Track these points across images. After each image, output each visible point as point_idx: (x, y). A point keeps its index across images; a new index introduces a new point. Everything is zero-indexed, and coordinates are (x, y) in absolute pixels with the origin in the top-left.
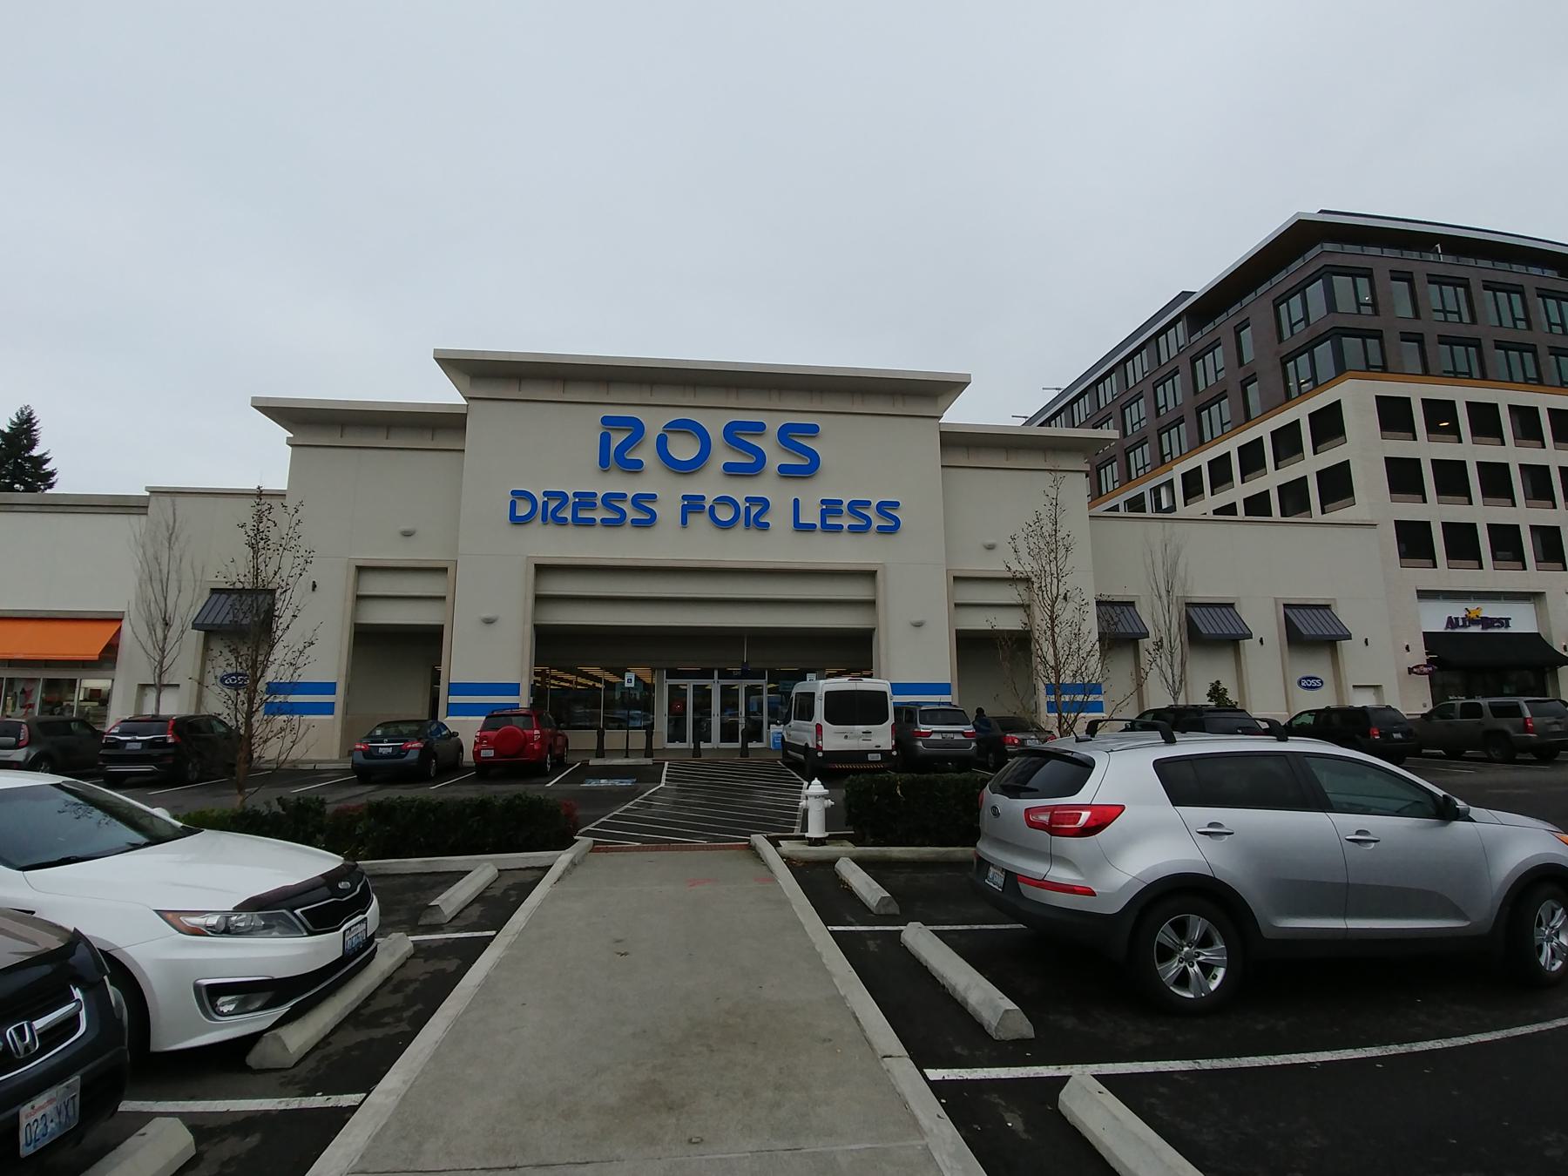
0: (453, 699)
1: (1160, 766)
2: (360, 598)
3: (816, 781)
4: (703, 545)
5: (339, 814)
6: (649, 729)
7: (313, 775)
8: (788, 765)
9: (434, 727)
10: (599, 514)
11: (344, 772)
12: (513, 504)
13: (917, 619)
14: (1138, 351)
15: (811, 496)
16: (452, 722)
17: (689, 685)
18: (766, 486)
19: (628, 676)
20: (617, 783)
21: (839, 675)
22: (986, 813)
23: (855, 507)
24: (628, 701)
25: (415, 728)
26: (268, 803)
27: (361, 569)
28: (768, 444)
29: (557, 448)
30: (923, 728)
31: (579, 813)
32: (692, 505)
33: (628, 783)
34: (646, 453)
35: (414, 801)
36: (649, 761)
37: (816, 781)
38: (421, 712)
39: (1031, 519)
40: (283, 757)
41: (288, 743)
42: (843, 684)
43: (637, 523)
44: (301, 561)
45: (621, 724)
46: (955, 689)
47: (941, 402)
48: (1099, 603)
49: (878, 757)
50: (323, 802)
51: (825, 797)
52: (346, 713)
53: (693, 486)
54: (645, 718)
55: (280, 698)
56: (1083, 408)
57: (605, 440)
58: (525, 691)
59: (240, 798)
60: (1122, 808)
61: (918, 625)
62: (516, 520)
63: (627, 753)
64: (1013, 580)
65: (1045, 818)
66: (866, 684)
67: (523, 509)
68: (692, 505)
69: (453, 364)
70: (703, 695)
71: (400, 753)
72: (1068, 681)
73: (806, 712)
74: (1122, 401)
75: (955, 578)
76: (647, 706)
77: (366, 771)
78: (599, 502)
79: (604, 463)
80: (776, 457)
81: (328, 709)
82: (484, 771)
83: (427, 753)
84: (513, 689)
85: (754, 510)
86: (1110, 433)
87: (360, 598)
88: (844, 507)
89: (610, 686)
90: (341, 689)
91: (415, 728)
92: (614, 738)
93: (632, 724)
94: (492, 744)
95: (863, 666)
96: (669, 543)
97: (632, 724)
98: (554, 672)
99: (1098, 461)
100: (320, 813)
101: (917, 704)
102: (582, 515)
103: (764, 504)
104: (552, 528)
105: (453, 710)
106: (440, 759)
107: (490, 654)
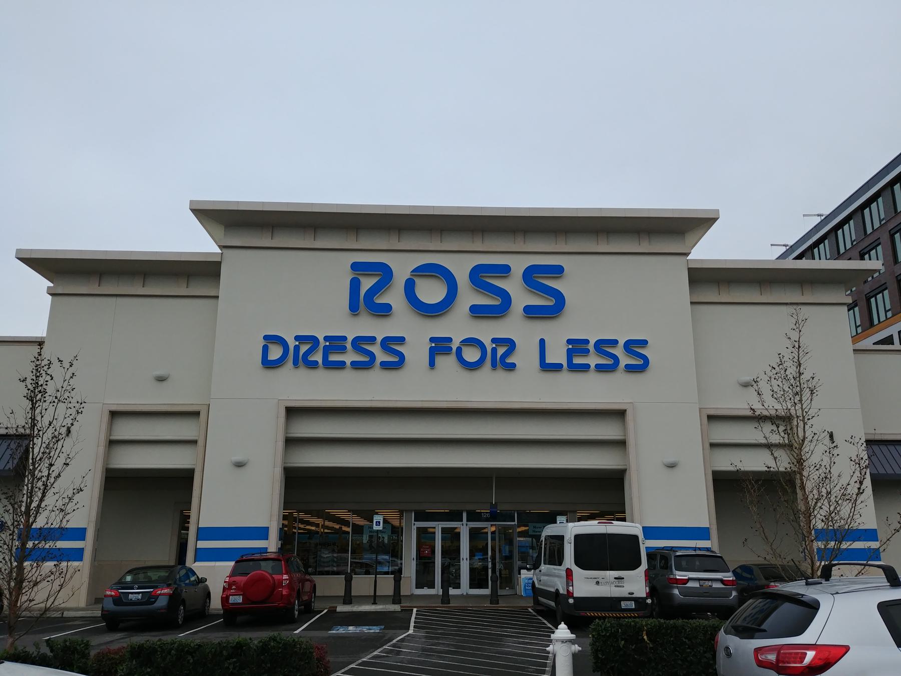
0: (202, 544)
1: (884, 608)
2: (112, 443)
3: (563, 626)
4: (450, 386)
5: (100, 657)
6: (398, 574)
7: (62, 622)
8: (539, 612)
9: (183, 572)
10: (349, 357)
11: (93, 620)
12: (265, 350)
13: (671, 460)
14: (846, 220)
15: (557, 336)
16: (201, 568)
17: (438, 527)
18: (512, 327)
19: (378, 518)
20: (365, 629)
21: (591, 517)
22: (721, 654)
23: (602, 346)
24: (377, 546)
25: (163, 574)
26: (37, 645)
27: (114, 415)
28: (513, 286)
29: (311, 294)
30: (680, 575)
31: (330, 658)
32: (440, 346)
33: (375, 630)
34: (394, 297)
35: (173, 643)
36: (397, 608)
37: (563, 626)
38: (167, 557)
39: (775, 362)
40: (847, 527)
41: (56, 587)
42: (592, 527)
43: (385, 366)
44: (73, 411)
45: (367, 569)
46: (714, 533)
47: (690, 238)
48: (869, 442)
49: (632, 605)
50: (87, 645)
51: (572, 642)
52: (95, 557)
53: (439, 328)
54: (393, 564)
55: (49, 545)
56: (849, 234)
57: (355, 285)
58: (274, 534)
59: (10, 640)
60: (846, 649)
61: (672, 466)
62: (268, 364)
63: (375, 599)
64: (773, 419)
65: (772, 657)
66: (617, 528)
67: (275, 353)
68: (440, 346)
69: (207, 214)
70: (452, 537)
71: (150, 599)
72: (820, 525)
73: (556, 558)
74: (891, 226)
75: (711, 418)
76: (395, 551)
77: (113, 621)
78: (349, 346)
79: (354, 308)
80: (521, 298)
81: (78, 554)
82: (232, 616)
83: (175, 599)
84: (262, 533)
85: (501, 351)
86: (874, 263)
87: (112, 443)
88: (591, 346)
89: (358, 530)
90: (90, 535)
91: (163, 574)
92: (362, 584)
93: (379, 569)
94: (242, 590)
95: (618, 512)
96: (416, 385)
97: (379, 569)
98: (302, 515)
99: (867, 289)
100: (85, 655)
101: (672, 549)
102: (333, 358)
103: (510, 344)
104: (303, 373)
105: (202, 555)
106: (188, 606)
107: (240, 497)
